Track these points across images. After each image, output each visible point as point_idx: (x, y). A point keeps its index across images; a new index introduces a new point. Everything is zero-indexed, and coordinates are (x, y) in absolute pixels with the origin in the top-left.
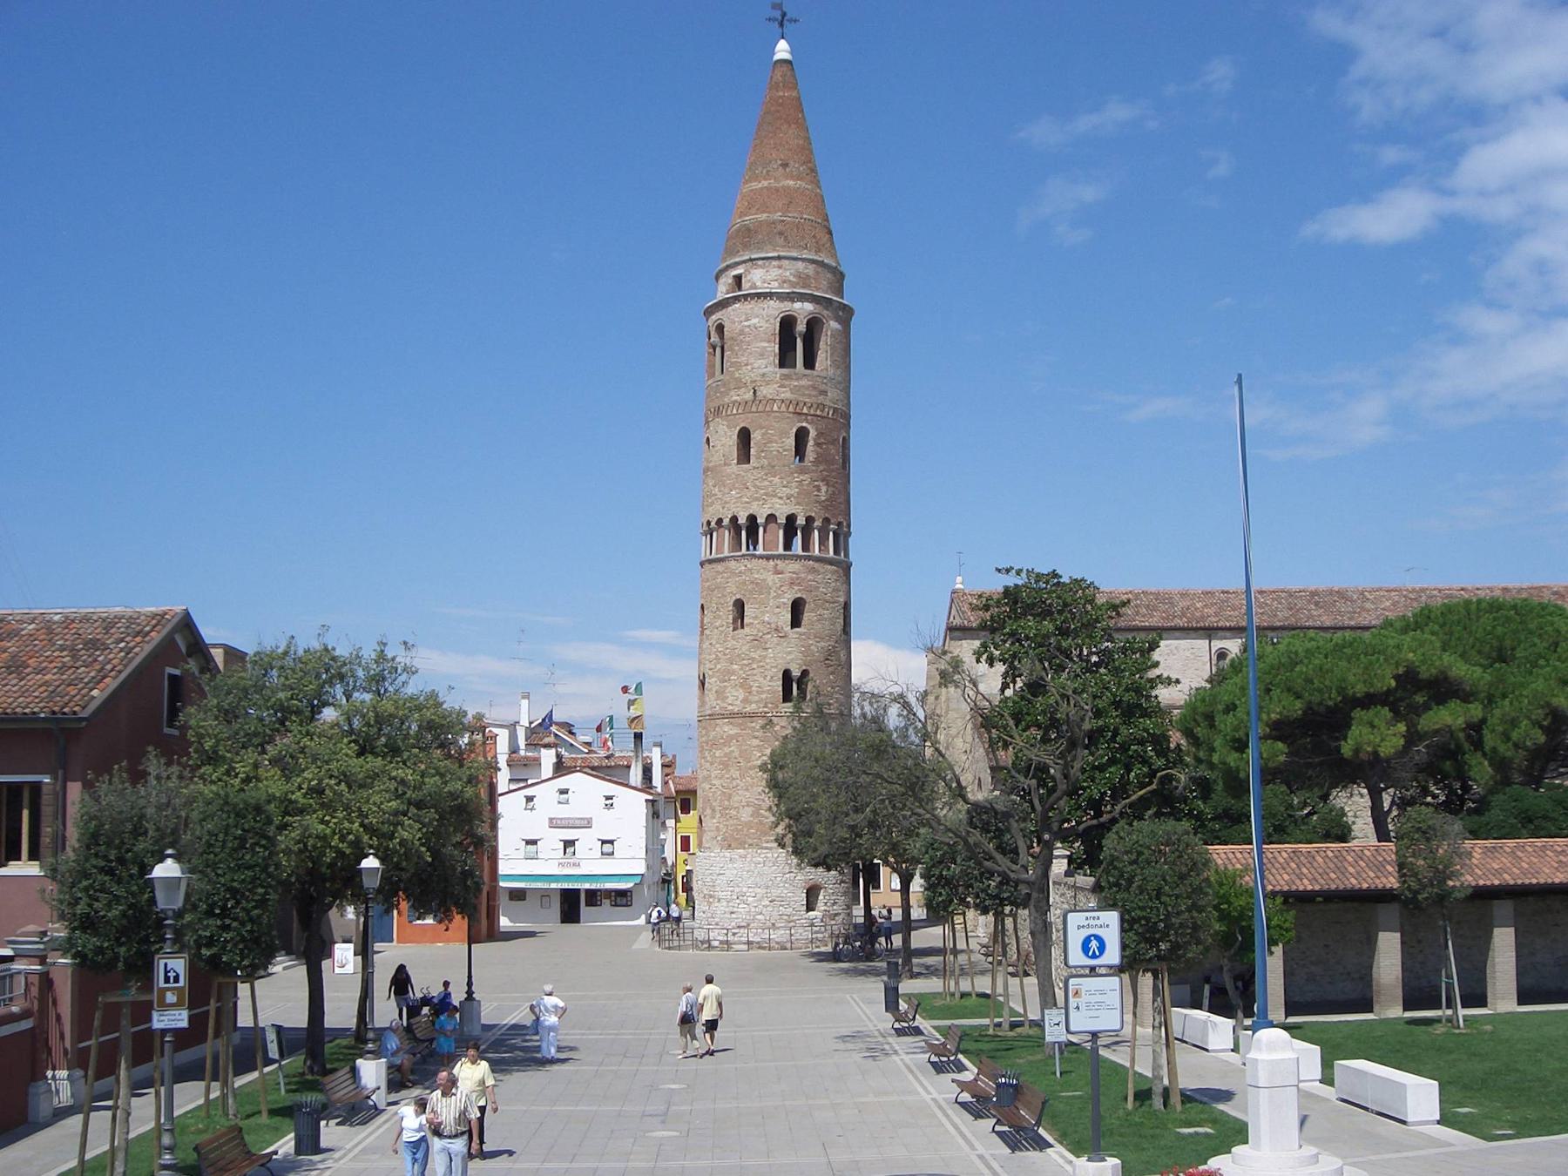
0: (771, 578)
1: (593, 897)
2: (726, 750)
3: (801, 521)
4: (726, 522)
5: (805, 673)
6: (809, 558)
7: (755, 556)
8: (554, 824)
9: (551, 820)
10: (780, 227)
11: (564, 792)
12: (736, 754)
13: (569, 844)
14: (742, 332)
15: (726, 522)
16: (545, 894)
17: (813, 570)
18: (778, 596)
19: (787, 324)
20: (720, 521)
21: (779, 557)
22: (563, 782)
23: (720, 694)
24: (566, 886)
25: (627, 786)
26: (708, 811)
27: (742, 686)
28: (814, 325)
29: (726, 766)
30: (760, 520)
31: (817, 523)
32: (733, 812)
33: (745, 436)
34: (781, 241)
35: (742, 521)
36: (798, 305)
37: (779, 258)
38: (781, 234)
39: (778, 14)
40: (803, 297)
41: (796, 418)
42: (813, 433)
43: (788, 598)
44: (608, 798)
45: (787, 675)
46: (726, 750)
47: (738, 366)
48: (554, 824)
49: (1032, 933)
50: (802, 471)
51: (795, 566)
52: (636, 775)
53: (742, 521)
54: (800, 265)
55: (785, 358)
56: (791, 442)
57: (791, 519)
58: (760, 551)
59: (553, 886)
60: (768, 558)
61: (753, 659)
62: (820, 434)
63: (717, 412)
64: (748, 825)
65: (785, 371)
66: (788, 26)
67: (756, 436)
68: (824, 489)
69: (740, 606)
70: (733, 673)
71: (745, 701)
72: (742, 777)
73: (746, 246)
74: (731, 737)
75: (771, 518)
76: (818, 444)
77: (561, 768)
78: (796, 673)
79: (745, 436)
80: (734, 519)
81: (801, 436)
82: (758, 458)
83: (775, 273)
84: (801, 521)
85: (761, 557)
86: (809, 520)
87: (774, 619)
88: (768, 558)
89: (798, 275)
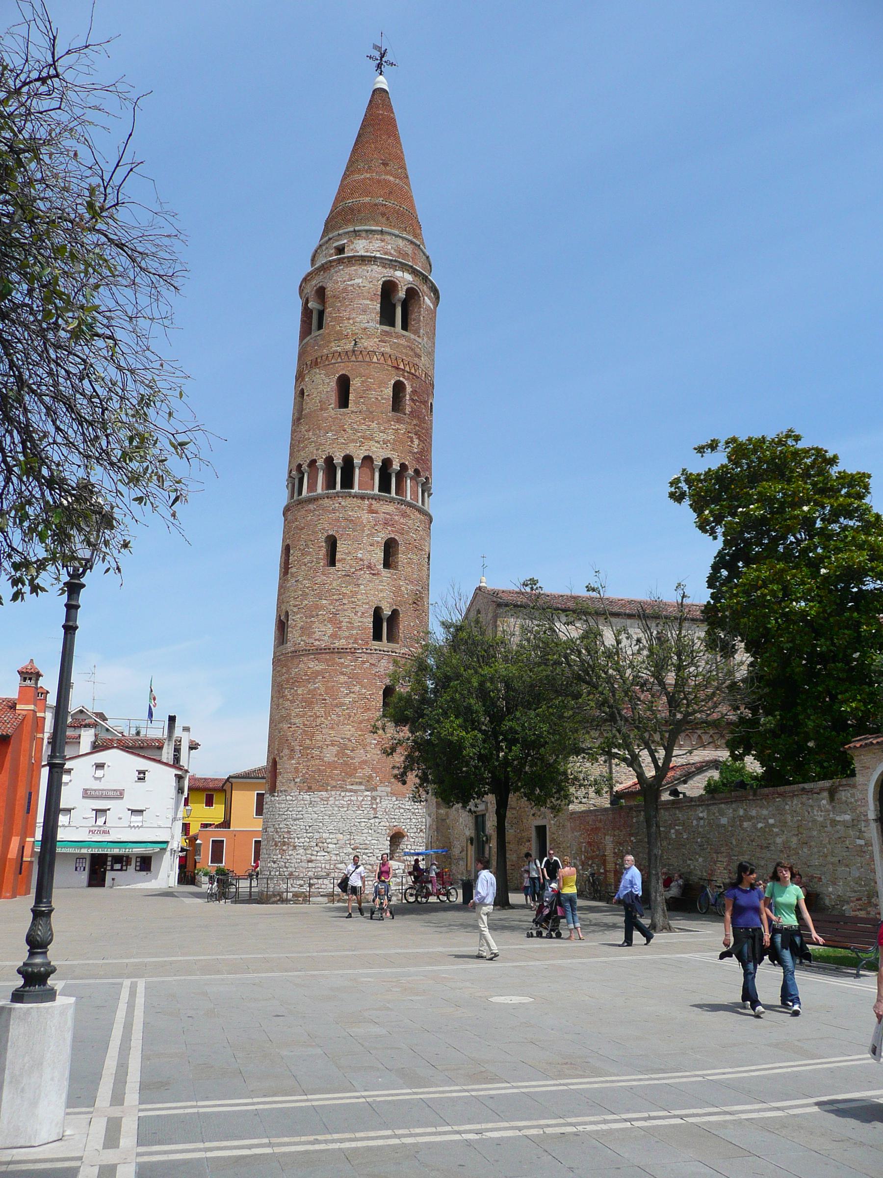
0: (366, 517)
1: (122, 860)
2: (311, 687)
3: (396, 466)
4: (320, 463)
5: (395, 613)
6: (403, 502)
7: (350, 495)
8: (87, 794)
9: (85, 790)
10: (382, 209)
11: (100, 766)
12: (322, 690)
13: (100, 812)
14: (345, 290)
15: (320, 463)
16: (80, 857)
17: (404, 515)
18: (372, 535)
19: (389, 288)
20: (313, 462)
21: (374, 497)
22: (100, 757)
23: (306, 630)
24: (96, 851)
25: (159, 762)
26: (286, 751)
27: (330, 621)
28: (412, 293)
29: (309, 704)
30: (357, 461)
31: (411, 472)
32: (316, 752)
33: (344, 384)
34: (384, 220)
35: (338, 460)
36: (399, 274)
37: (382, 232)
38: (383, 214)
39: (377, 54)
40: (404, 267)
41: (394, 371)
42: (409, 389)
43: (381, 538)
44: (140, 772)
45: (378, 611)
46: (311, 687)
47: (339, 320)
48: (87, 794)
49: (417, 872)
50: (399, 421)
51: (391, 508)
52: (167, 754)
53: (338, 460)
54: (401, 243)
55: (387, 317)
56: (389, 392)
57: (387, 462)
58: (356, 490)
59: (84, 851)
60: (363, 497)
61: (344, 594)
62: (414, 392)
63: (315, 363)
64: (332, 765)
65: (387, 328)
66: (386, 68)
67: (356, 384)
68: (416, 442)
69: (332, 543)
70: (322, 607)
71: (334, 636)
72: (327, 715)
73: (347, 222)
74: (317, 673)
75: (368, 459)
76: (412, 399)
77: (97, 747)
78: (387, 612)
79: (344, 384)
80: (329, 460)
81: (398, 388)
82: (357, 403)
83: (377, 244)
84: (396, 466)
85: (355, 496)
86: (403, 467)
87: (367, 557)
88: (363, 497)
89: (399, 251)
